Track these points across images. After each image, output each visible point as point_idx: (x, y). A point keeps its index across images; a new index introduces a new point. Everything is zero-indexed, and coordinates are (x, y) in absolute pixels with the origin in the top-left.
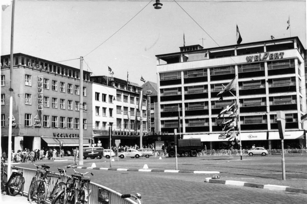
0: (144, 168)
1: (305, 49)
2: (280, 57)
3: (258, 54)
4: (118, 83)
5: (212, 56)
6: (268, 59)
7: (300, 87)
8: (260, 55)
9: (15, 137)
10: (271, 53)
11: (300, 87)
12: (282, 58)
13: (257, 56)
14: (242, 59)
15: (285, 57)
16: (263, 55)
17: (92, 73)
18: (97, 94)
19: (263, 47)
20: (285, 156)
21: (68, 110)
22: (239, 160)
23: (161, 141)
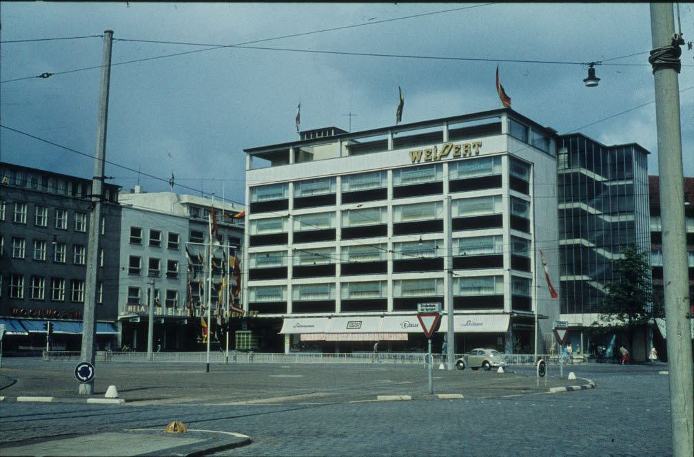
0: (106, 395)
1: (546, 126)
2: (473, 154)
3: (430, 147)
4: (287, 148)
5: (355, 150)
6: (451, 157)
7: (149, 294)
8: (436, 147)
9: (685, 176)
10: (456, 143)
11: (149, 294)
12: (477, 154)
13: (429, 152)
14: (403, 157)
15: (483, 152)
16: (440, 147)
17: (121, 187)
18: (136, 232)
19: (441, 133)
20: (559, 369)
21: (73, 264)
22: (204, 371)
23: (434, 332)
